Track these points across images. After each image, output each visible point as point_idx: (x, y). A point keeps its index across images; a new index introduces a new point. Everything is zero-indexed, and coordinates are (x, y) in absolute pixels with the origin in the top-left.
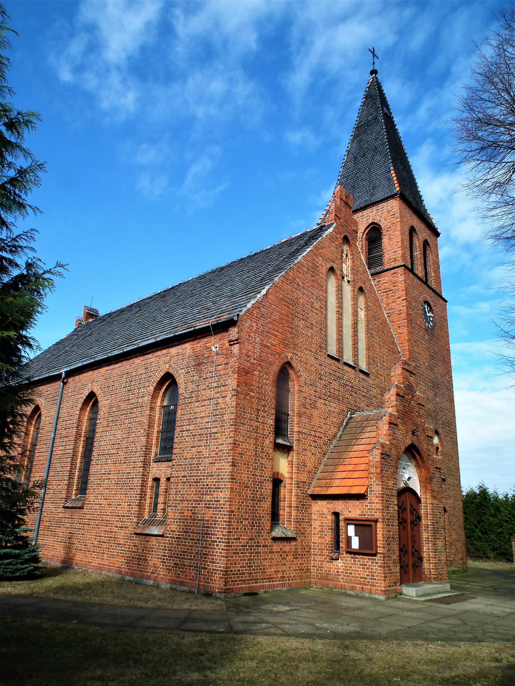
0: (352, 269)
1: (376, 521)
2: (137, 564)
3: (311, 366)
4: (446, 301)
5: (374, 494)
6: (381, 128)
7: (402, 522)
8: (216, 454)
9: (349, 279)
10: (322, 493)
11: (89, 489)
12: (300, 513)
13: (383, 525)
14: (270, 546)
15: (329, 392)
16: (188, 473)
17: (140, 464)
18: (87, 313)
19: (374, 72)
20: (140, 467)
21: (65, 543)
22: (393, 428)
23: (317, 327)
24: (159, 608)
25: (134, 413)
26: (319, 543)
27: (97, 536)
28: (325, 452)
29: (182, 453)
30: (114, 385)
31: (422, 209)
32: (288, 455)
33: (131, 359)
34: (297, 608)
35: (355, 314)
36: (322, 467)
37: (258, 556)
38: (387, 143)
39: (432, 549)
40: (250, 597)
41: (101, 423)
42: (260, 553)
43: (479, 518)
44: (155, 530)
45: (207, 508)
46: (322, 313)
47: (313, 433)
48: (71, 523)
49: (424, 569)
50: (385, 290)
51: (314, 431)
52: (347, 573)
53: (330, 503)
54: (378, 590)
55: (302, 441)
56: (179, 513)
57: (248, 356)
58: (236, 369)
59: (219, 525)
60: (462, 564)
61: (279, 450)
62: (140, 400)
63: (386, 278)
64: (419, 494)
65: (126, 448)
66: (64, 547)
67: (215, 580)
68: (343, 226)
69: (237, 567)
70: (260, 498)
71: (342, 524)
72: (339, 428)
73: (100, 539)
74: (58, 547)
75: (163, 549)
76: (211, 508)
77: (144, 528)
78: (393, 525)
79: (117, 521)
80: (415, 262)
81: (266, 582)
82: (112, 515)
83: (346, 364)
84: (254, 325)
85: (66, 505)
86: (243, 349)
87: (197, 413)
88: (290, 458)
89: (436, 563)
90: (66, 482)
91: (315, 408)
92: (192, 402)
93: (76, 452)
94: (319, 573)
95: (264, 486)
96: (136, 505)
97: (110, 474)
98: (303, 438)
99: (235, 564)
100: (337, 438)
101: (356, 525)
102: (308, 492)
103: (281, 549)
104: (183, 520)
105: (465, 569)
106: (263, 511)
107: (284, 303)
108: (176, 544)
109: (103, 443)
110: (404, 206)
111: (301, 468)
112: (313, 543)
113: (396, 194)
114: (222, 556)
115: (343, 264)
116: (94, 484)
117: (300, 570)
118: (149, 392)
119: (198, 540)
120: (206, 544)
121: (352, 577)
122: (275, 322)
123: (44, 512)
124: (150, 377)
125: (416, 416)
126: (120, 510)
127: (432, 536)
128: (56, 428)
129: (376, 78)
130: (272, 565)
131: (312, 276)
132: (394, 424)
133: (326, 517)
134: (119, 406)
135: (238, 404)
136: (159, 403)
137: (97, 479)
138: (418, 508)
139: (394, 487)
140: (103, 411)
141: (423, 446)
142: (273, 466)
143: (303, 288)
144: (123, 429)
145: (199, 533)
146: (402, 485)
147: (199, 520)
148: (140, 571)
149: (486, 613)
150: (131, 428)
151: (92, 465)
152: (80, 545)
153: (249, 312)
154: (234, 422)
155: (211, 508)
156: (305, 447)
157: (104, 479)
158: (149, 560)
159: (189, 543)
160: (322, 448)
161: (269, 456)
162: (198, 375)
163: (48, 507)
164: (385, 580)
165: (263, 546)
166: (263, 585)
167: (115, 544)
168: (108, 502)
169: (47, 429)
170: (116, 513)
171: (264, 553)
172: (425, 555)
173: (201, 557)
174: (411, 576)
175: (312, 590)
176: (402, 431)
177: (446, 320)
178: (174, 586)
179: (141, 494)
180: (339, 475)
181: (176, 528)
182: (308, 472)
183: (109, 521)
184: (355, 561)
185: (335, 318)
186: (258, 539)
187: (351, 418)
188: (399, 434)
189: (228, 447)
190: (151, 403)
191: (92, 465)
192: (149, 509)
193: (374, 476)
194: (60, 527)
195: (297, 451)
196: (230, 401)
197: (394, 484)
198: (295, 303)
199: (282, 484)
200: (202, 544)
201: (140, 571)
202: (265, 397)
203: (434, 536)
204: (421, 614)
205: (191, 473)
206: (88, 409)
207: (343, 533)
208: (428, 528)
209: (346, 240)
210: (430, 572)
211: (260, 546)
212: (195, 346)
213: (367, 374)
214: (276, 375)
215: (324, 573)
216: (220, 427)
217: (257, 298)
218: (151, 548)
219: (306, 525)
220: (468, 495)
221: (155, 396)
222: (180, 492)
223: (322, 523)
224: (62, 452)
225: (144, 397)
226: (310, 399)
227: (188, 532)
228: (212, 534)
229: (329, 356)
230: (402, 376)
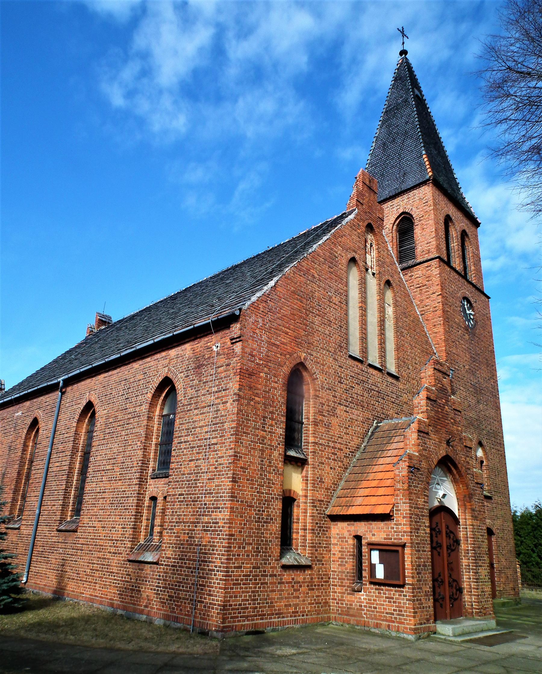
0: (378, 261)
1: (404, 546)
2: (131, 596)
3: (329, 367)
4: (489, 298)
5: (401, 514)
6: (412, 111)
7: (435, 547)
8: (216, 468)
9: (375, 272)
10: (341, 513)
11: (83, 510)
12: (317, 537)
13: (412, 550)
14: (279, 575)
15: (350, 397)
16: (185, 491)
17: (136, 481)
18: (99, 319)
19: (404, 52)
20: (136, 484)
21: (58, 570)
22: (423, 437)
23: (336, 324)
24: (141, 651)
25: (131, 423)
26: (339, 572)
27: (90, 563)
28: (347, 466)
29: (179, 468)
30: (111, 394)
31: (459, 197)
32: (303, 470)
33: (129, 364)
34: (305, 650)
35: (382, 310)
36: (342, 483)
37: (264, 587)
38: (418, 126)
40: (254, 636)
41: (97, 436)
42: (267, 583)
43: (536, 541)
44: (149, 557)
45: (205, 530)
46: (342, 308)
47: (331, 444)
48: (64, 548)
49: (465, 602)
50: (418, 286)
51: (333, 442)
52: (370, 607)
53: (351, 524)
54: (406, 628)
55: (318, 453)
56: (176, 537)
57: (253, 356)
58: (238, 371)
59: (217, 550)
60: (514, 595)
61: (291, 464)
62: (138, 409)
63: (418, 272)
64: (457, 514)
65: (122, 463)
66: (56, 576)
67: (212, 616)
68: (366, 213)
69: (238, 601)
70: (267, 519)
71: (365, 549)
72: (363, 438)
73: (93, 567)
74: (50, 575)
75: (158, 579)
76: (209, 531)
77: (138, 554)
78: (425, 551)
79: (110, 546)
80: (452, 254)
81: (275, 618)
82: (106, 540)
83: (371, 366)
84: (260, 320)
85: (60, 528)
86: (246, 347)
87: (195, 421)
88: (304, 472)
89: (478, 596)
90: (61, 502)
91: (334, 416)
92: (191, 410)
93: (73, 468)
94: (339, 607)
95: (272, 505)
96: (131, 528)
97: (105, 492)
98: (320, 450)
99: (236, 597)
100: (361, 450)
101: (380, 551)
102: (326, 512)
103: (293, 579)
104: (179, 545)
105: (518, 600)
106: (271, 534)
107: (297, 296)
108: (172, 573)
109: (99, 458)
110: (437, 192)
111: (318, 484)
112: (332, 571)
113: (428, 180)
114: (220, 588)
115: (367, 255)
116: (88, 504)
117: (317, 603)
118: (147, 400)
119: (195, 568)
120: (203, 574)
121: (377, 612)
122: (285, 318)
123: (38, 535)
124: (148, 382)
126: (114, 534)
127: (473, 563)
128: (53, 442)
129: (406, 58)
130: (282, 598)
131: (329, 267)
132: (424, 433)
133: (347, 541)
134: (116, 417)
135: (240, 411)
136: (157, 413)
137: (91, 499)
138: (456, 529)
139: (425, 506)
140: (100, 422)
141: (460, 458)
142: (282, 482)
143: (319, 280)
144: (120, 441)
145: (195, 561)
146: (436, 504)
147: (196, 545)
148: (132, 604)
149: (536, 657)
150: (127, 440)
151: (88, 483)
152: (73, 573)
153: (254, 306)
154: (236, 431)
155: (209, 531)
156: (322, 460)
157: (99, 498)
158: (143, 591)
159: (185, 571)
160: (342, 462)
161: (278, 470)
162: (197, 379)
163: (42, 530)
164: (414, 617)
165: (271, 576)
166: (271, 622)
167: (108, 572)
168: (102, 524)
169: (44, 443)
170: (109, 537)
171: (271, 583)
172: (465, 585)
173: (198, 589)
174: (448, 611)
175: (331, 628)
176: (434, 440)
177: (489, 319)
178: (168, 623)
179: (136, 515)
180: (362, 492)
181: (172, 555)
182: (326, 489)
183: (102, 545)
184: (379, 593)
185: (358, 315)
186: (265, 567)
187: (377, 427)
188: (431, 444)
189: (228, 460)
190: (149, 411)
191: (88, 483)
192: (145, 532)
193: (401, 493)
194: (53, 553)
195: (313, 464)
196: (231, 407)
197: (424, 502)
198: (310, 297)
199: (296, 503)
200: (199, 573)
201: (132, 604)
202: (273, 402)
203: (475, 563)
204: (456, 659)
205: (188, 491)
206: (87, 420)
207: (366, 559)
208: (468, 553)
209: (370, 228)
210: (472, 605)
211: (267, 576)
212: (195, 346)
213: (396, 378)
214: (287, 378)
215: (345, 608)
216: (220, 437)
217: (264, 291)
218: (145, 577)
219: (323, 550)
220: (522, 516)
221: (153, 404)
222: (176, 512)
223: (342, 548)
224: (58, 469)
225: (142, 405)
226: (328, 406)
227: (184, 559)
228: (210, 562)
229: (351, 357)
230: (433, 378)
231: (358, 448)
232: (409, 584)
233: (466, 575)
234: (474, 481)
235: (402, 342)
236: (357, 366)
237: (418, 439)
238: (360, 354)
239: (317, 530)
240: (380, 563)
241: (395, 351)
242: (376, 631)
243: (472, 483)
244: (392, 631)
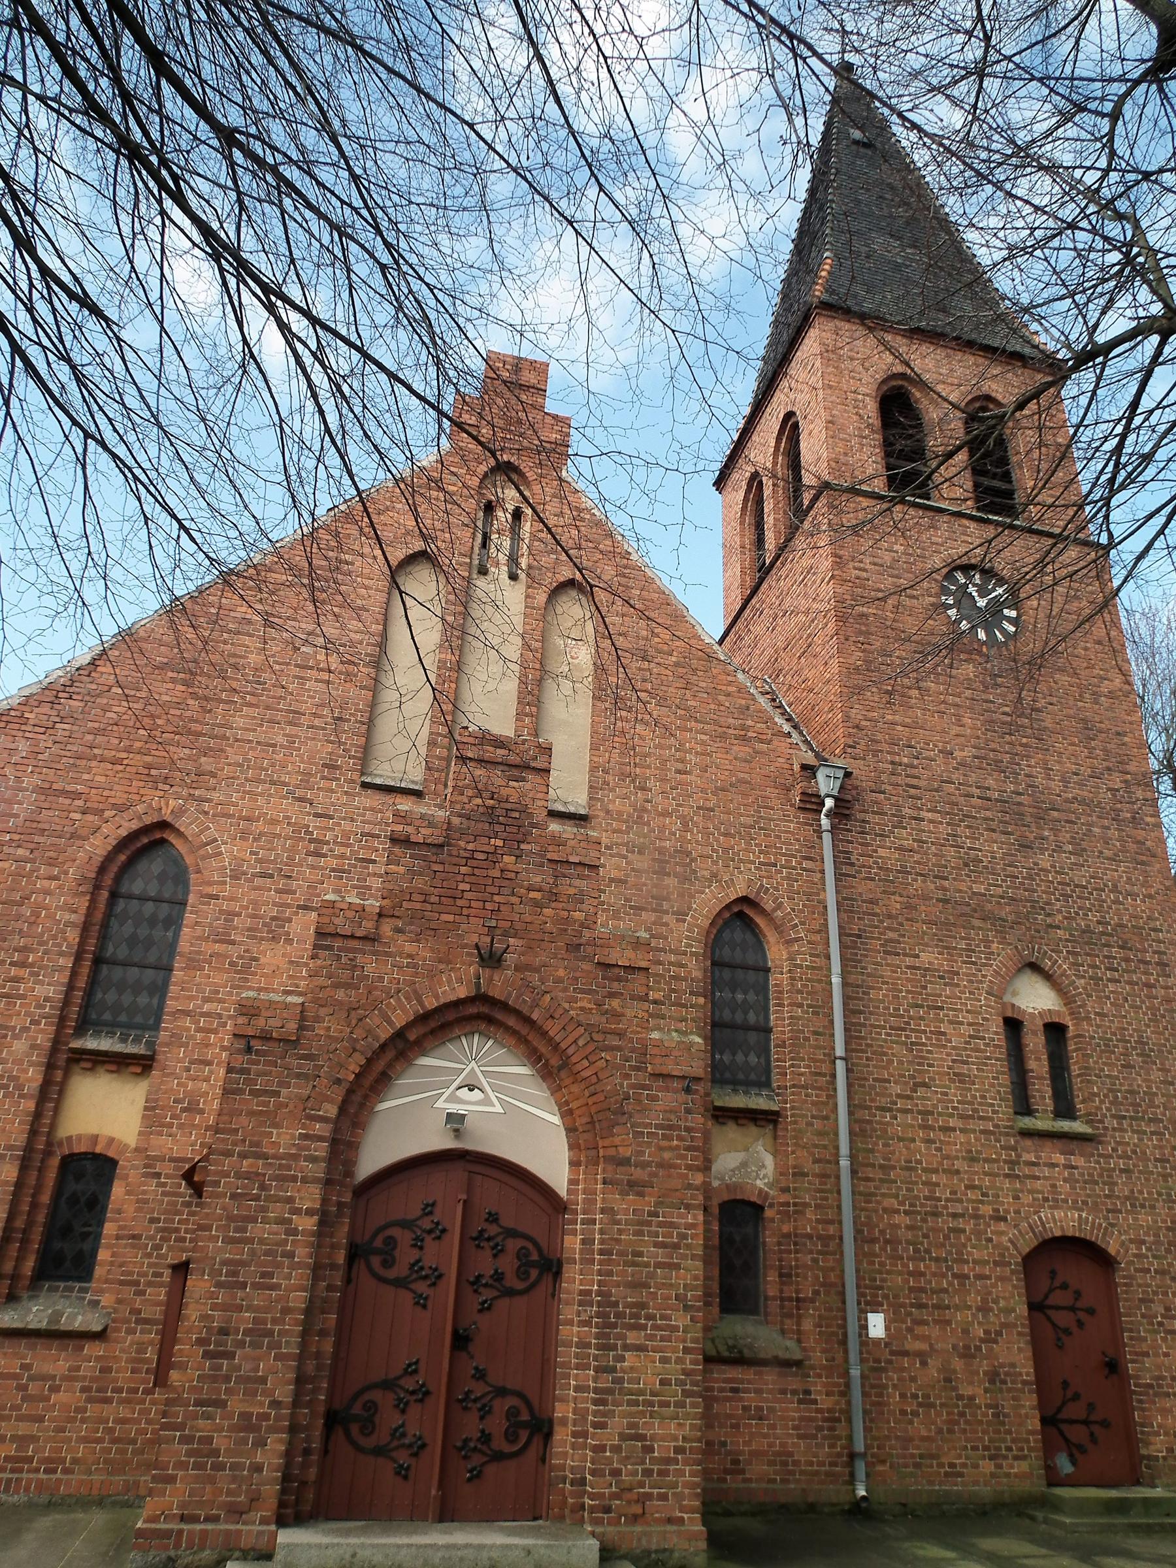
12: (149, 1255)
98: (199, 1030)
239: (152, 1238)
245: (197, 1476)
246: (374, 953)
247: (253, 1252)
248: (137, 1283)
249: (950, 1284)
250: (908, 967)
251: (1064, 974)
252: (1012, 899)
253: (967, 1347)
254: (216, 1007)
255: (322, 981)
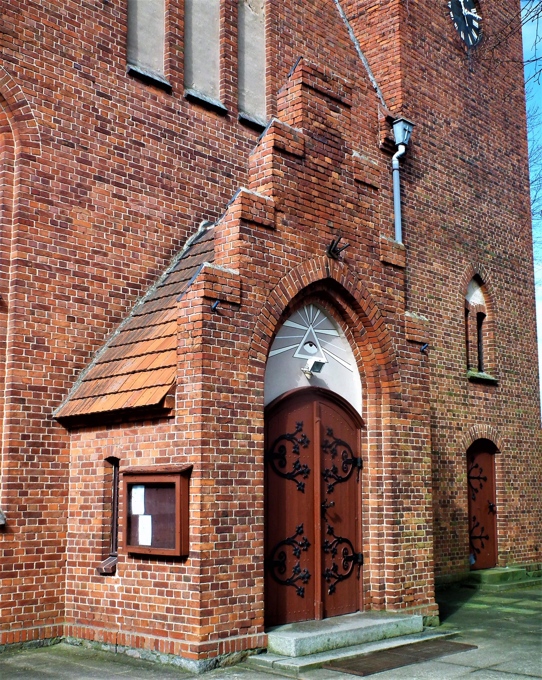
3: (67, 94)
12: (26, 465)
15: (132, 165)
28: (117, 314)
39: (388, 535)
55: (31, 285)
72: (168, 257)
94: (79, 607)
98: (36, 279)
101: (148, 486)
121: (140, 615)
125: (349, 211)
127: (388, 504)
133: (94, 472)
146: (303, 383)
160: (105, 306)
164: (201, 623)
184: (145, 576)
223: (87, 487)
229: (133, 74)
231: (153, 278)
232: (194, 554)
233: (374, 529)
234: (403, 337)
235: (287, 57)
236: (155, 98)
237: (241, 238)
238: (166, 73)
239: (26, 451)
240: (146, 514)
241: (267, 75)
242: (136, 653)
243: (397, 341)
244: (162, 652)
245: (223, 608)
246: (274, 239)
247: (234, 460)
248: (20, 486)
249: (439, 467)
250: (428, 271)
251: (489, 283)
252: (472, 232)
253: (444, 501)
254: (47, 260)
255: (247, 258)
